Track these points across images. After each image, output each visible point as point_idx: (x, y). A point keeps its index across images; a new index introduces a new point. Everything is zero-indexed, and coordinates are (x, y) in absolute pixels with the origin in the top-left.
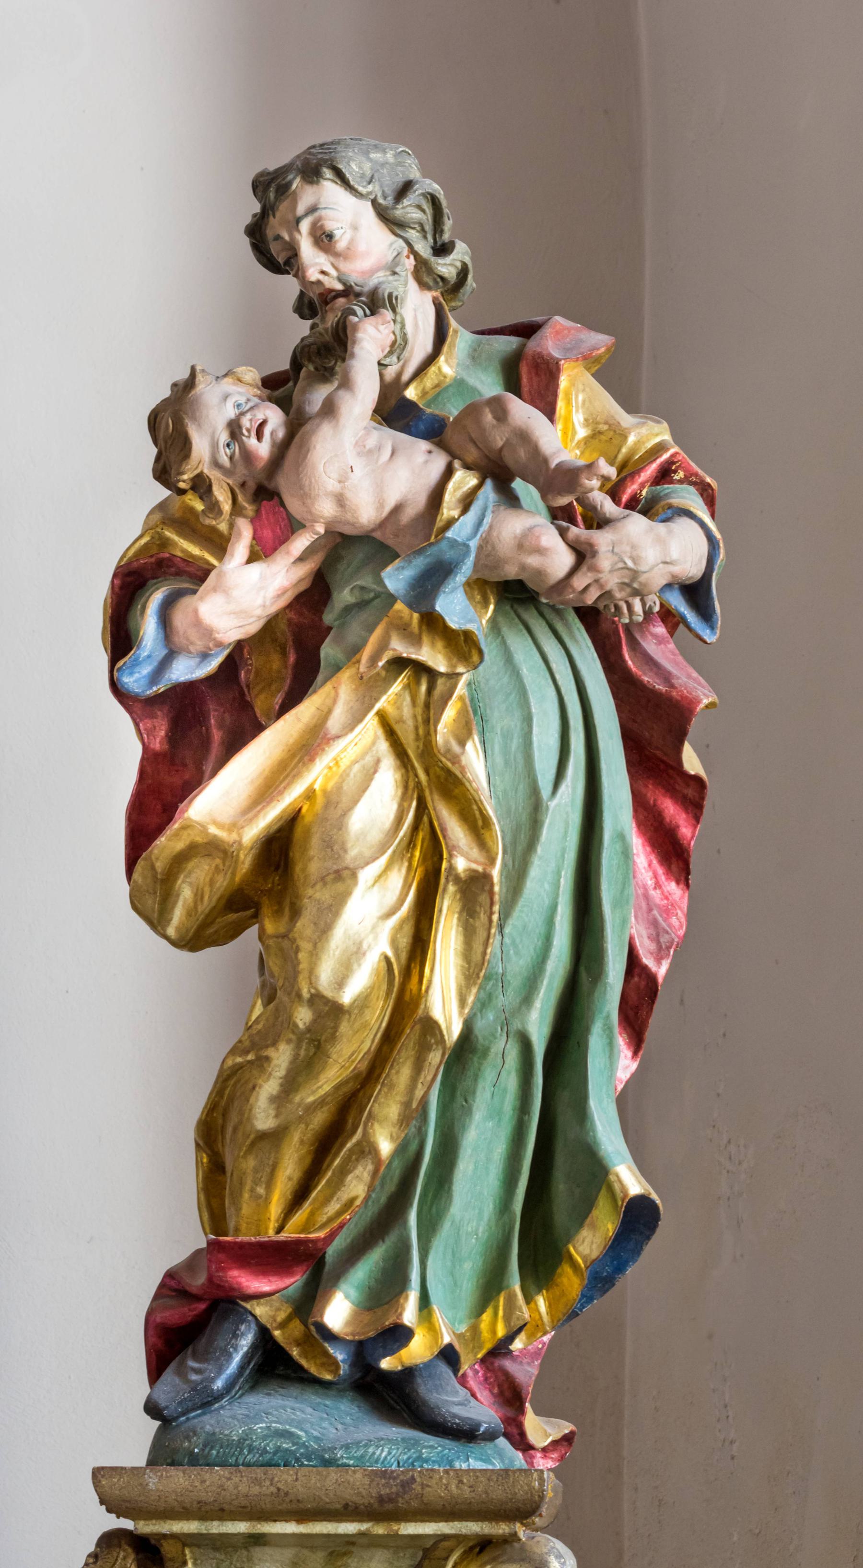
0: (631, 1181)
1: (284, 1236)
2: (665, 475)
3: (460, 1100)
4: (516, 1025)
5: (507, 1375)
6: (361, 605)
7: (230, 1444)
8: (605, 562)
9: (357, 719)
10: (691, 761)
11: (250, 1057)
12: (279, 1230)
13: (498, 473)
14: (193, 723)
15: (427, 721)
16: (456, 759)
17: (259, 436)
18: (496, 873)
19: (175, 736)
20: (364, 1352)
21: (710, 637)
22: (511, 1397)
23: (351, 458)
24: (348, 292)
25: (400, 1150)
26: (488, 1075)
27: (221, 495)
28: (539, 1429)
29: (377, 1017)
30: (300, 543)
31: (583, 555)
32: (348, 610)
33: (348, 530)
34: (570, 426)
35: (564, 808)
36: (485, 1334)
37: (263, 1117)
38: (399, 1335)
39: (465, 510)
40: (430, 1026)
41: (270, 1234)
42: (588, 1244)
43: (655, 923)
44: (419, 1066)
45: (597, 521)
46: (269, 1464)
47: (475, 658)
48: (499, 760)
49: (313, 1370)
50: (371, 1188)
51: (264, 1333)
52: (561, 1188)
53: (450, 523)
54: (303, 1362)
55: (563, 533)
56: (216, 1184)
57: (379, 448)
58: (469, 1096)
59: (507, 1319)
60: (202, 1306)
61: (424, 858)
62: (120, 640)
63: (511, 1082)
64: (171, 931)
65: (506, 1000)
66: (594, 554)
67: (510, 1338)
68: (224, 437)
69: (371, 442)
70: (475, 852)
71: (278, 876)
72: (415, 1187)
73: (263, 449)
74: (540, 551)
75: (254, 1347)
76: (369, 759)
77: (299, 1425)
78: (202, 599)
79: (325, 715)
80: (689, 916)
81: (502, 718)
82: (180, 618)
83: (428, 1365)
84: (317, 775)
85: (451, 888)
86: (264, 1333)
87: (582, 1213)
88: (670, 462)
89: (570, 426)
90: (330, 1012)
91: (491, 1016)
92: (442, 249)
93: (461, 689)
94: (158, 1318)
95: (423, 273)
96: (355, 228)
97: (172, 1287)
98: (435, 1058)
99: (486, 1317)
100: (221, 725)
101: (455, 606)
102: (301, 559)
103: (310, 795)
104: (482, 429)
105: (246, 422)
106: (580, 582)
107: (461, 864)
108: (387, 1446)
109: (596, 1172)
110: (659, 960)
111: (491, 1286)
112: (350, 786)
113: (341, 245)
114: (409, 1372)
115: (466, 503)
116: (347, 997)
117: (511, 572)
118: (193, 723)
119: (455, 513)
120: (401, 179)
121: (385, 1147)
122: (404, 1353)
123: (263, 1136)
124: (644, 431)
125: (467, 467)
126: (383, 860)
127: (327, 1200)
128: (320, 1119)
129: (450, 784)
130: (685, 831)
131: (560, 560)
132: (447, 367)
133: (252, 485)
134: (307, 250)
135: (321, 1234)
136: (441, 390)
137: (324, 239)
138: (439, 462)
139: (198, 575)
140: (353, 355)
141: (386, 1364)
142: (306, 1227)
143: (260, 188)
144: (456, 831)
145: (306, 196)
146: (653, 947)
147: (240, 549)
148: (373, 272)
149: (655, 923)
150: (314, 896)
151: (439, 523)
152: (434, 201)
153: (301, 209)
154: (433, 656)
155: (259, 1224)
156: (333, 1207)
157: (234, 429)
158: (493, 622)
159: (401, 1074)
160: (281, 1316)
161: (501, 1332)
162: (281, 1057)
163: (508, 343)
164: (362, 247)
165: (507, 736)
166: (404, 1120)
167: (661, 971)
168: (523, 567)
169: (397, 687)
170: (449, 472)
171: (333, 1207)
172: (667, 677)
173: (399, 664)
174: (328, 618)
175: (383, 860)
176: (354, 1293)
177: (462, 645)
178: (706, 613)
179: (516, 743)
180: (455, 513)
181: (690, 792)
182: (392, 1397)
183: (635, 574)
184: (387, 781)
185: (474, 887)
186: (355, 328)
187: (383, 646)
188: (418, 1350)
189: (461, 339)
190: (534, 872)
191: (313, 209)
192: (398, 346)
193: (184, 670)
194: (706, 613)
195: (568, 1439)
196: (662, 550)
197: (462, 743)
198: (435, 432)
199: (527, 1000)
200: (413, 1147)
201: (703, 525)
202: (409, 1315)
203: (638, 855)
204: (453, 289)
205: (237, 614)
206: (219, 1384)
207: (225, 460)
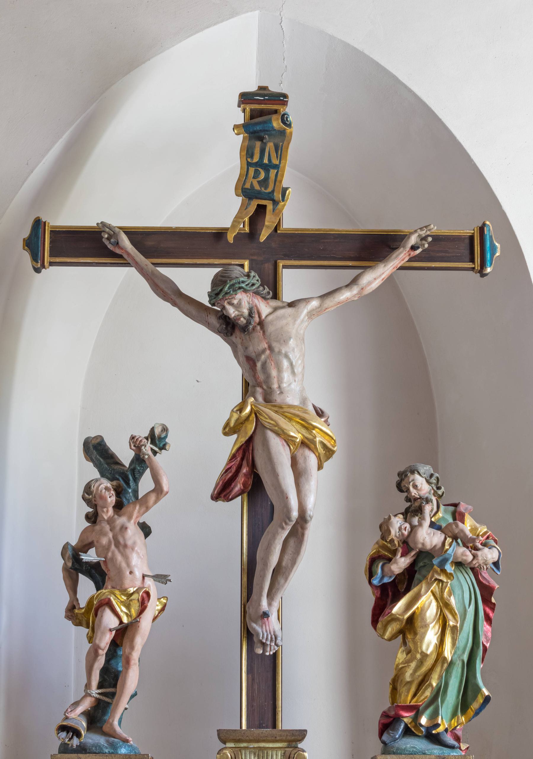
0: (487, 693)
1: (411, 704)
2: (488, 538)
3: (449, 674)
4: (461, 658)
5: (456, 734)
6: (424, 566)
7: (402, 749)
8: (480, 558)
9: (427, 592)
10: (493, 600)
11: (406, 665)
12: (410, 703)
13: (455, 538)
15: (442, 592)
16: (449, 601)
17: (405, 530)
18: (458, 625)
19: (382, 594)
20: (429, 729)
21: (499, 573)
22: (457, 739)
23: (426, 536)
24: (420, 498)
25: (437, 685)
26: (455, 669)
27: (396, 543)
28: (463, 746)
29: (434, 657)
30: (413, 553)
31: (475, 557)
32: (421, 567)
33: (423, 550)
35: (471, 610)
36: (453, 725)
37: (408, 677)
38: (437, 725)
39: (450, 547)
40: (445, 659)
41: (408, 704)
42: (475, 706)
43: (485, 635)
44: (442, 667)
45: (476, 549)
46: (411, 754)
47: (452, 578)
48: (457, 601)
49: (417, 733)
50: (431, 693)
51: (406, 725)
52: (470, 693)
53: (447, 550)
54: (415, 731)
55: (470, 551)
57: (431, 533)
58: (451, 673)
59: (457, 722)
60: (392, 719)
61: (442, 622)
63: (460, 670)
64: (386, 637)
65: (459, 652)
66: (477, 556)
67: (457, 726)
68: (398, 530)
69: (429, 532)
70: (454, 620)
71: (411, 626)
73: (406, 533)
74: (466, 556)
75: (404, 728)
76: (429, 600)
77: (416, 745)
78: (391, 565)
79: (420, 591)
80: (492, 633)
81: (458, 591)
82: (386, 569)
83: (442, 732)
84: (419, 604)
85: (449, 628)
86: (406, 725)
87: (475, 697)
88: (489, 535)
90: (425, 656)
91: (456, 656)
92: (439, 488)
93: (449, 585)
94: (382, 722)
95: (435, 493)
96: (422, 484)
97: (385, 715)
98: (446, 665)
99: (453, 721)
100: (391, 591)
101: (449, 568)
102: (413, 556)
103: (418, 608)
104: (452, 529)
105: (403, 527)
106: (474, 562)
107: (451, 623)
109: (478, 690)
110: (487, 643)
111: (454, 714)
112: (426, 606)
113: (419, 488)
114: (438, 734)
115: (450, 545)
116: (429, 653)
117: (460, 560)
119: (448, 547)
120: (430, 473)
121: (434, 684)
122: (439, 729)
123: (408, 682)
124: (482, 527)
125: (449, 537)
126: (435, 622)
127: (421, 696)
128: (420, 678)
129: (447, 605)
130: (491, 615)
131: (470, 558)
132: (440, 514)
133: (403, 541)
134: (411, 489)
135: (421, 704)
136: (439, 519)
137: (415, 487)
138: (443, 536)
139: (390, 560)
140: (424, 513)
141: (434, 732)
142: (416, 702)
143: (400, 476)
144: (450, 616)
145: (411, 477)
146: (485, 640)
147: (399, 555)
148: (426, 494)
149: (485, 635)
150: (420, 631)
151: (445, 550)
152: (438, 478)
153: (410, 480)
154: (443, 578)
155: (405, 701)
156: (422, 698)
157: (400, 529)
158: (454, 570)
159: (438, 669)
160: (410, 722)
161: (456, 725)
162: (413, 665)
163: (452, 508)
164: (423, 488)
165: (459, 595)
166: (438, 679)
167: (488, 645)
168: (462, 559)
169: (435, 585)
170: (445, 539)
171: (422, 698)
172: (488, 582)
173: (436, 579)
174: (416, 568)
175: (435, 622)
176: (427, 716)
177: (450, 576)
178: (498, 568)
179: (460, 597)
180: (448, 547)
181: (492, 606)
183: (486, 561)
184: (434, 604)
185: (454, 629)
186: (424, 506)
187: (433, 576)
188: (441, 729)
189: (442, 508)
190: (465, 625)
191: (413, 480)
192: (432, 511)
193: (386, 580)
194: (498, 568)
195: (468, 748)
197: (450, 597)
198: (439, 528)
199: (464, 652)
200: (440, 684)
201: (498, 549)
202: (440, 721)
204: (440, 497)
205: (399, 568)
206: (397, 736)
207: (398, 535)
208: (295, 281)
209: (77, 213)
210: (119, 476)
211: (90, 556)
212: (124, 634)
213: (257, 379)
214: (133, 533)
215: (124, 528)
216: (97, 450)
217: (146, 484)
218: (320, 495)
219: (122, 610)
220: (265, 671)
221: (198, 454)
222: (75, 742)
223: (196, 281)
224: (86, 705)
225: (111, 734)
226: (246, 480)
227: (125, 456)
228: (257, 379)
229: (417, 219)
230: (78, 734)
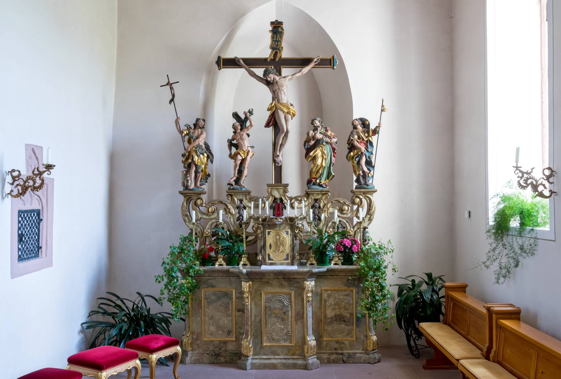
13: (326, 136)
14: (309, 150)
20: (319, 183)
34: (329, 133)
56: (311, 174)
62: (305, 145)
71: (314, 158)
72: (322, 174)
89: (329, 133)
90: (318, 165)
97: (308, 180)
101: (324, 143)
108: (321, 188)
111: (325, 180)
118: (309, 150)
182: (321, 186)
196: (335, 140)
203: (520, 193)
208: (285, 71)
209: (229, 54)
210: (241, 122)
211: (235, 142)
212: (243, 161)
213: (276, 97)
214: (245, 136)
215: (243, 135)
216: (236, 116)
217: (248, 124)
218: (293, 127)
219: (242, 155)
220: (279, 170)
221: (260, 117)
222: (232, 187)
223: (260, 72)
224: (234, 178)
225: (241, 185)
226: (273, 122)
227: (243, 117)
228: (276, 97)
229: (317, 55)
230: (232, 185)
